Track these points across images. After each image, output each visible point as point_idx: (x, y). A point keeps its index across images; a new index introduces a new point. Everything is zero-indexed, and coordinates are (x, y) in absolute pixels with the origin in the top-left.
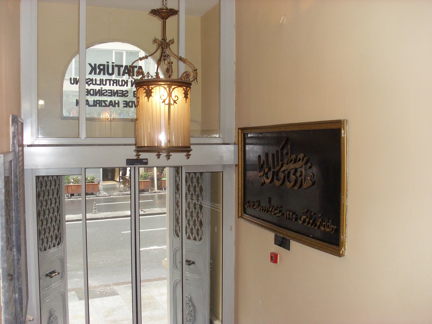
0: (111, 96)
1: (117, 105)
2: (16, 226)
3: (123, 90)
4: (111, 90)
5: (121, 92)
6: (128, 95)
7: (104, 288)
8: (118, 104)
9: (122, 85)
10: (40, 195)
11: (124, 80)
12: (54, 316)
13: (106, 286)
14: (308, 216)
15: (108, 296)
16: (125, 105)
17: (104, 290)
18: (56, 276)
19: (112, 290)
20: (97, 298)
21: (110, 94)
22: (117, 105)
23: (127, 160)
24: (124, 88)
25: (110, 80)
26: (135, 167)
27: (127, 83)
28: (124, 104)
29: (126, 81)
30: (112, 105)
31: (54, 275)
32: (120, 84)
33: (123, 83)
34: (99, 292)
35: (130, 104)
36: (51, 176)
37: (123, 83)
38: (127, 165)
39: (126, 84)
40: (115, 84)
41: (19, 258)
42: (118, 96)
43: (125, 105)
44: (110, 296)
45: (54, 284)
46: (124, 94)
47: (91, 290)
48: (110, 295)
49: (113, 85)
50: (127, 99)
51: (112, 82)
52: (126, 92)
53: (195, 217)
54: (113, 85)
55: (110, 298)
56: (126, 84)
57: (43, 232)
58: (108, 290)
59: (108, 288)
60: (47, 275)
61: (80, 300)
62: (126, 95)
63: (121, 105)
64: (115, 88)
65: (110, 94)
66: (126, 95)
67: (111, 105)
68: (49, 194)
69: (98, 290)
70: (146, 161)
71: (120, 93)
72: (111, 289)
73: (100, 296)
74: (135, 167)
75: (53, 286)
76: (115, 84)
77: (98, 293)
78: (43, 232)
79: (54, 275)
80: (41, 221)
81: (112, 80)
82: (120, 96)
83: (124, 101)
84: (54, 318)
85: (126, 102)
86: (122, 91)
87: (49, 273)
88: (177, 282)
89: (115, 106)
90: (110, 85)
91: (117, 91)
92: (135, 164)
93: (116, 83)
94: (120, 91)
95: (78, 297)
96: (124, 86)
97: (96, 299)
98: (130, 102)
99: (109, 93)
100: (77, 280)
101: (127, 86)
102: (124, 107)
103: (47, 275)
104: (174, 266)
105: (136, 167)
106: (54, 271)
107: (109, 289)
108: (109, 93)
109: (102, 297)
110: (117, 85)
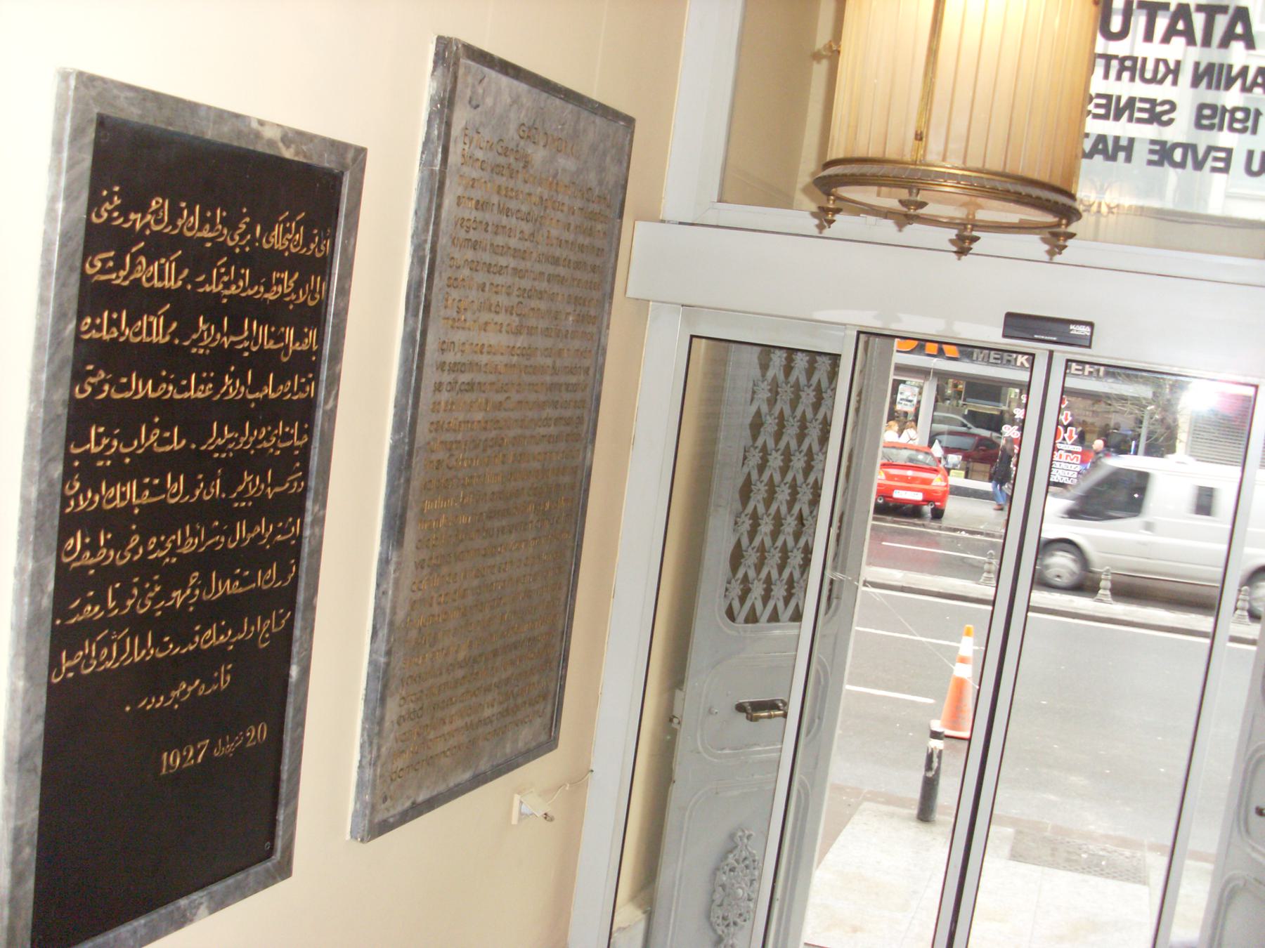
0: (1105, 117)
1: (1122, 155)
2: (397, 437)
3: (1155, 100)
4: (1108, 97)
5: (1147, 106)
6: (1171, 121)
7: (1114, 848)
8: (1129, 148)
9: (1154, 80)
10: (762, 424)
11: (1166, 62)
12: (744, 854)
13: (1124, 842)
14: (1141, 422)
15: (1107, 877)
16: (1155, 158)
17: (1108, 852)
18: (774, 720)
19: (1135, 864)
20: (1071, 870)
21: (1102, 111)
22: (1122, 155)
23: (1010, 317)
24: (1159, 92)
25: (1108, 58)
26: (1051, 353)
27: (1175, 72)
28: (1152, 152)
29: (1172, 66)
30: (1104, 152)
31: (766, 714)
32: (1148, 75)
33: (1162, 68)
34: (1090, 854)
35: (1178, 155)
36: (758, 349)
37: (1162, 68)
38: (1005, 336)
39: (1170, 77)
40: (1126, 75)
41: (388, 554)
42: (1130, 119)
43: (1155, 158)
44: (1114, 878)
45: (765, 746)
46: (1157, 114)
47: (1068, 842)
48: (1115, 875)
49: (1119, 77)
50: (1171, 134)
51: (1115, 64)
52: (1167, 107)
53: (777, 451)
54: (1119, 77)
55: (1112, 886)
56: (1170, 77)
57: (751, 558)
58: (1122, 857)
59: (1127, 853)
60: (740, 708)
61: (1010, 859)
62: (1165, 118)
63: (1141, 153)
64: (1125, 89)
65: (1102, 111)
66: (1165, 118)
67: (1099, 152)
68: (806, 431)
69: (1091, 847)
70: (1085, 330)
71: (1141, 110)
72: (1134, 857)
73: (1083, 869)
74: (1051, 353)
75: (759, 752)
76: (1126, 75)
77: (1084, 856)
78: (751, 558)
79: (766, 714)
80: (750, 519)
81: (1115, 57)
82: (1140, 121)
83: (1153, 142)
84: (745, 859)
85: (1162, 144)
86: (1153, 102)
87: (752, 704)
88: (1234, 887)
89: (1113, 158)
90: (1106, 76)
91: (1132, 101)
92: (1036, 336)
93: (1132, 70)
94: (1143, 100)
95: (1012, 849)
96: (1161, 82)
97: (1061, 873)
98: (1176, 145)
99: (1098, 106)
100: (1052, 797)
101: (1175, 83)
102: (1150, 163)
103: (740, 708)
104: (1238, 820)
105: (1055, 354)
106: (777, 702)
107: (1127, 858)
108: (1098, 106)
109: (1089, 872)
110: (1132, 79)
